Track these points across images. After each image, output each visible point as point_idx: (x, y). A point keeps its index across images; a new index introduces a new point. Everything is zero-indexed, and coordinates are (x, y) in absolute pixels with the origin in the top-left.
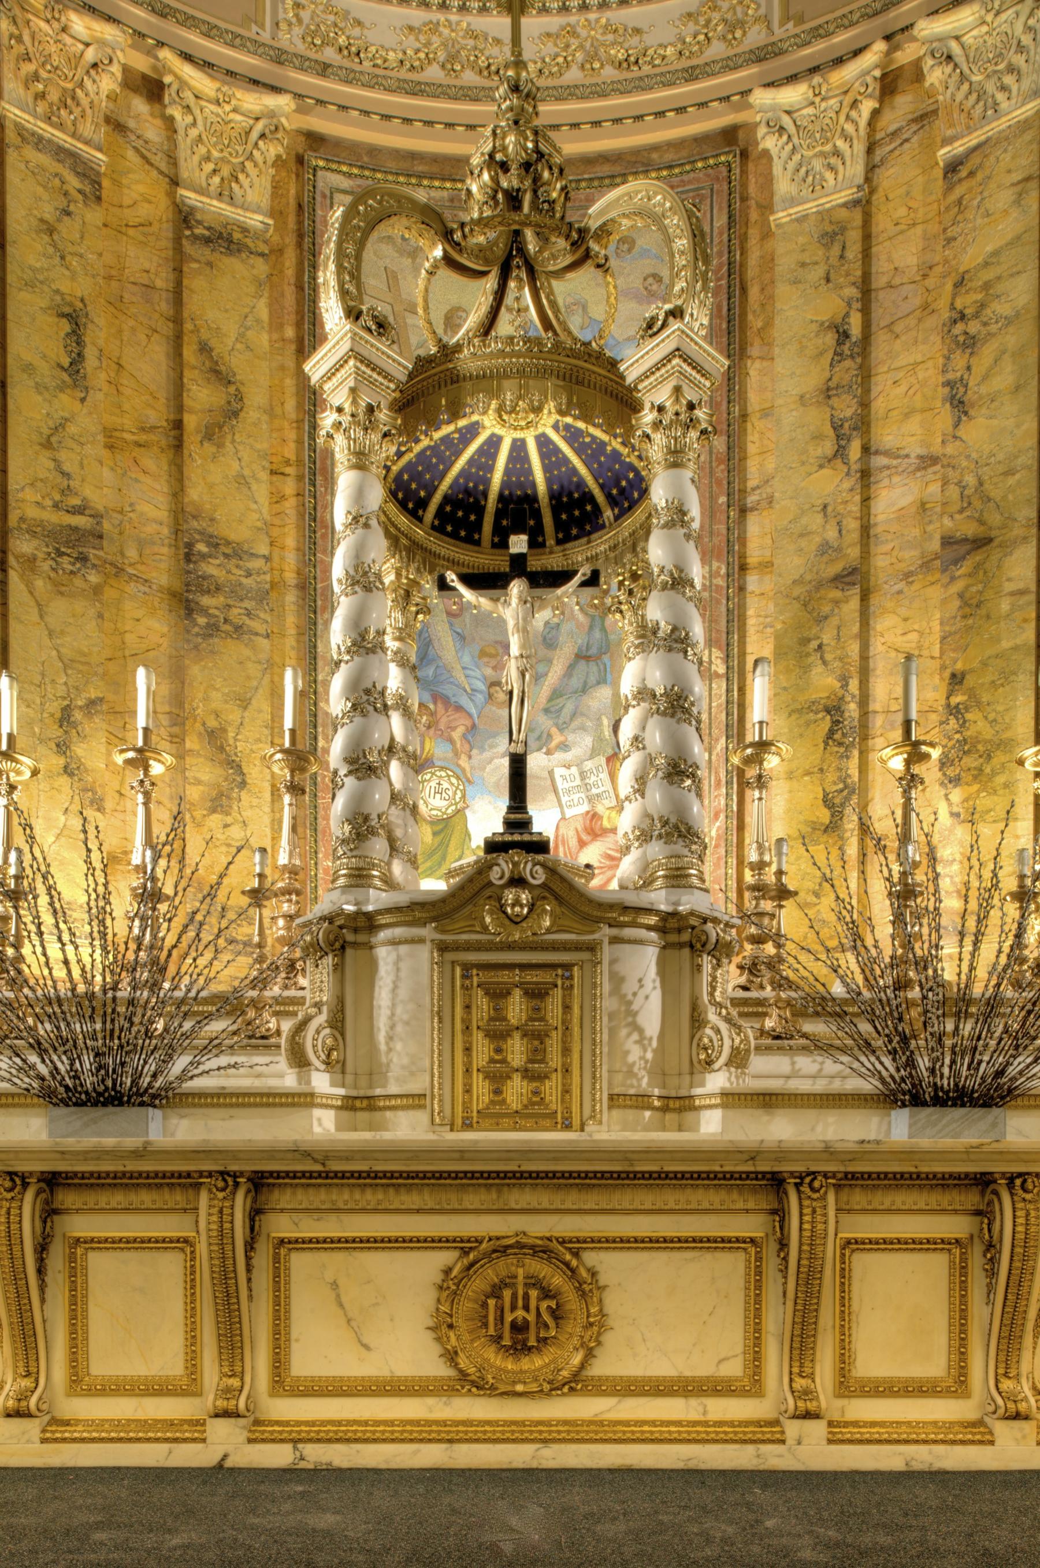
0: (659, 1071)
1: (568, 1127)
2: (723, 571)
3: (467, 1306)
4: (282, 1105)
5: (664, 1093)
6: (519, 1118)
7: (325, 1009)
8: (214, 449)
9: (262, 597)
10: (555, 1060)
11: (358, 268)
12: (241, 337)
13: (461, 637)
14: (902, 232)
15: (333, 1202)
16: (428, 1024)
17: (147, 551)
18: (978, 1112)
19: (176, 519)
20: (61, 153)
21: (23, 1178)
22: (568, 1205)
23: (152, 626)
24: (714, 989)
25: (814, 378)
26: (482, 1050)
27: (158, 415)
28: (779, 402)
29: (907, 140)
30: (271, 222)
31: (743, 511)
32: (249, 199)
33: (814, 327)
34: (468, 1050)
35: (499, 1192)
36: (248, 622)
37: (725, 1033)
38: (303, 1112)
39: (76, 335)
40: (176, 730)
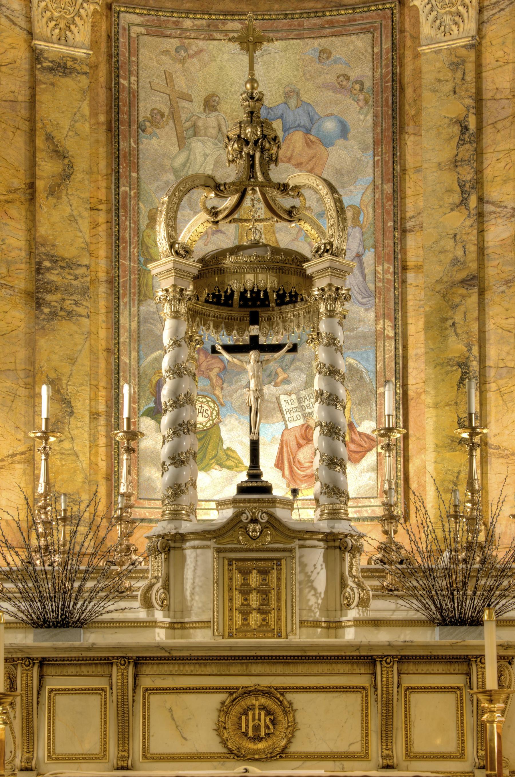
0: (325, 609)
1: (280, 637)
2: (391, 270)
3: (232, 719)
4: (141, 627)
5: (327, 620)
6: (255, 632)
7: (161, 580)
8: (55, 201)
9: (85, 292)
10: (273, 604)
11: (175, 224)
12: (72, 127)
14: (500, 66)
15: (171, 671)
16: (212, 587)
17: (12, 268)
18: (472, 628)
19: (30, 245)
21: (33, 660)
22: (279, 672)
24: (351, 569)
25: (447, 153)
26: (238, 599)
27: (19, 182)
28: (425, 166)
29: (502, 10)
30: (91, 52)
31: (404, 232)
32: (77, 39)
33: (446, 121)
34: (231, 600)
35: (247, 666)
36: (76, 308)
37: (356, 590)
38: (151, 630)
40: (29, 380)
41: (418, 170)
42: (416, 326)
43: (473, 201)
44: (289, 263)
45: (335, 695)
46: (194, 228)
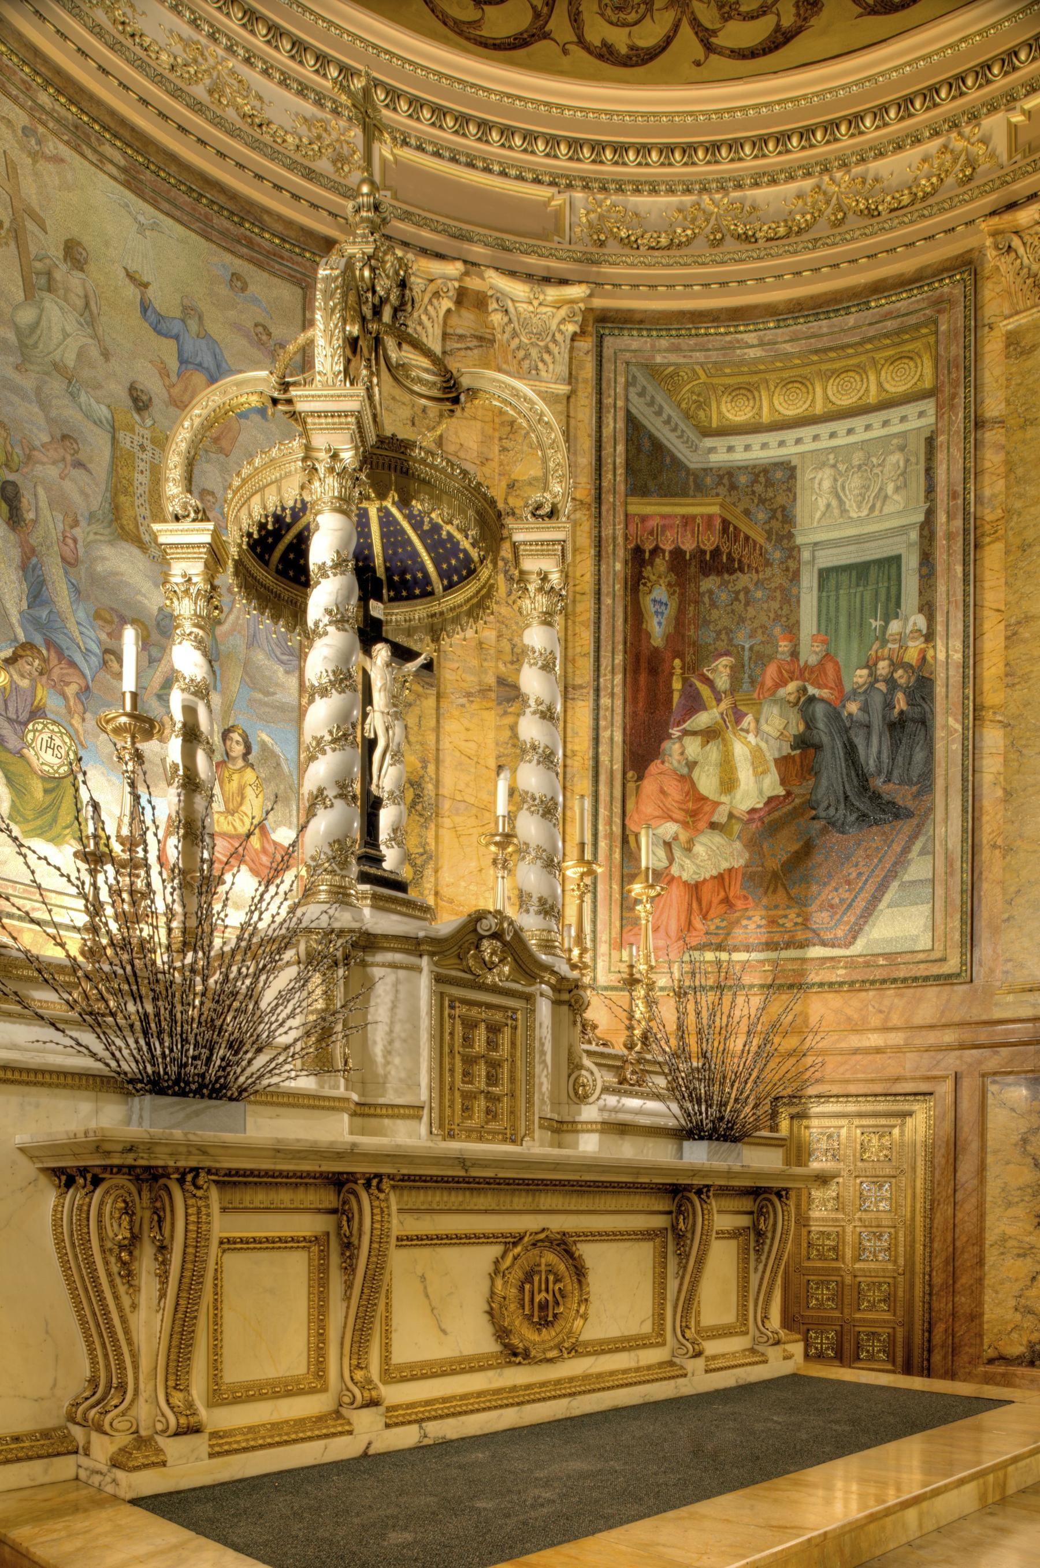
13: (76, 589)
45: (628, 1244)
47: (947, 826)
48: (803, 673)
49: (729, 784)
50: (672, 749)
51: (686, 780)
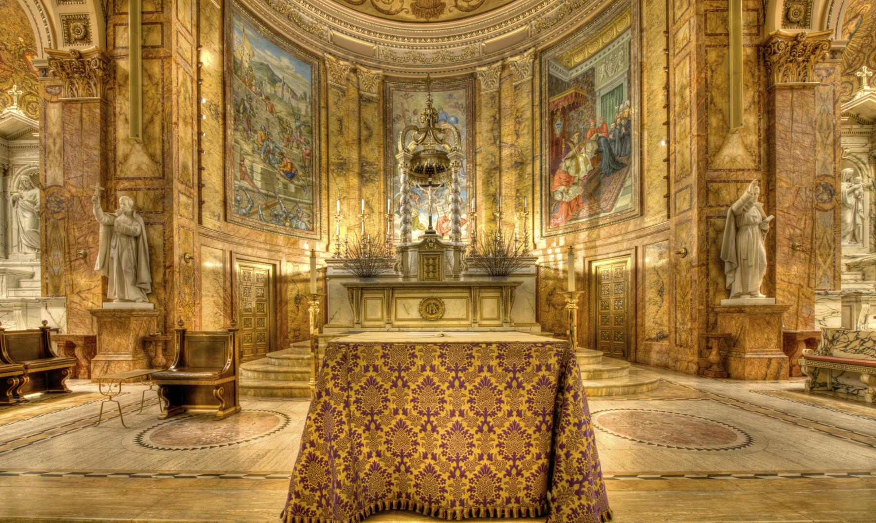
0: (454, 271)
20: (338, 88)
23: (354, 181)
27: (356, 137)
39: (341, 124)
41: (480, 133)
42: (479, 183)
43: (498, 142)
44: (442, 156)
46: (411, 146)
47: (635, 168)
48: (599, 130)
49: (578, 170)
50: (563, 166)
51: (567, 173)
